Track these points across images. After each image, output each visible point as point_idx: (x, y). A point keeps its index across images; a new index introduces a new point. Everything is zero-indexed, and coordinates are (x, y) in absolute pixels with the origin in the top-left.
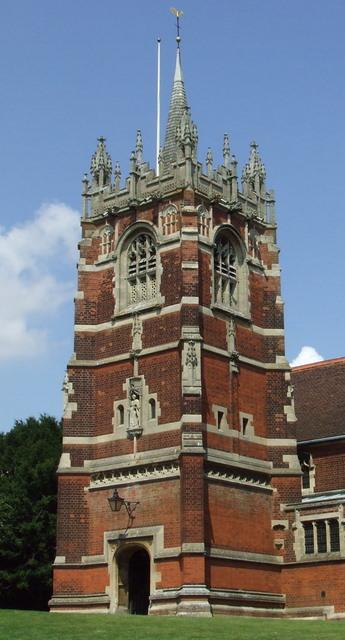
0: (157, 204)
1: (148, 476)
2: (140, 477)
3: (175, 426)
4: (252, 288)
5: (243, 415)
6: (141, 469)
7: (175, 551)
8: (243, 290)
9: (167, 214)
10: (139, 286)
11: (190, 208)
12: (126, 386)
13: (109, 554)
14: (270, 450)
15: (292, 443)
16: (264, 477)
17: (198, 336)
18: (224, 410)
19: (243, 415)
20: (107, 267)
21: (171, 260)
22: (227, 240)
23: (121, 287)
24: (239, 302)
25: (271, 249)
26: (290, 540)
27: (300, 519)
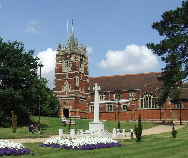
0: (71, 54)
1: (69, 98)
2: (67, 98)
3: (74, 91)
4: (84, 68)
5: (83, 89)
6: (68, 97)
7: (74, 110)
8: (83, 69)
9: (73, 56)
10: (67, 67)
11: (77, 56)
12: (65, 84)
13: (62, 110)
14: (86, 94)
15: (89, 94)
16: (85, 99)
17: (78, 77)
18: (83, 89)
19: (83, 89)
20: (61, 63)
21: (73, 64)
22: (81, 60)
23: (64, 67)
24: (82, 70)
25: (87, 61)
26: (88, 109)
27: (90, 106)
